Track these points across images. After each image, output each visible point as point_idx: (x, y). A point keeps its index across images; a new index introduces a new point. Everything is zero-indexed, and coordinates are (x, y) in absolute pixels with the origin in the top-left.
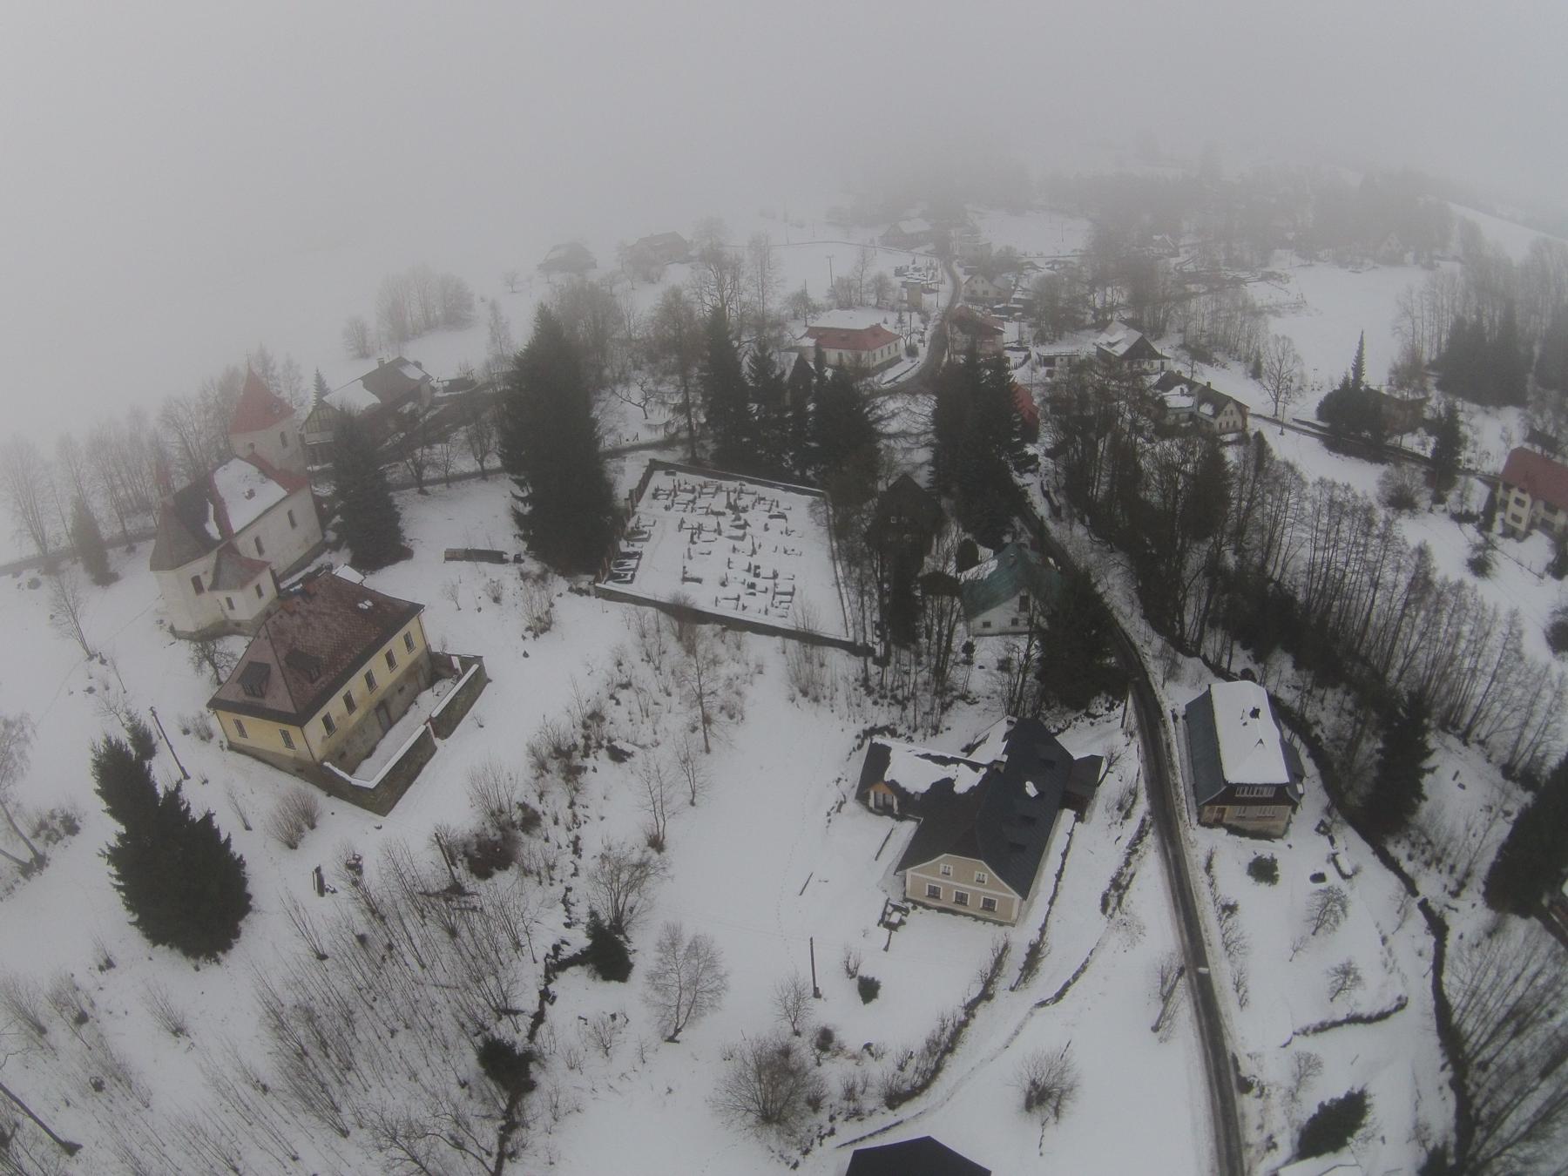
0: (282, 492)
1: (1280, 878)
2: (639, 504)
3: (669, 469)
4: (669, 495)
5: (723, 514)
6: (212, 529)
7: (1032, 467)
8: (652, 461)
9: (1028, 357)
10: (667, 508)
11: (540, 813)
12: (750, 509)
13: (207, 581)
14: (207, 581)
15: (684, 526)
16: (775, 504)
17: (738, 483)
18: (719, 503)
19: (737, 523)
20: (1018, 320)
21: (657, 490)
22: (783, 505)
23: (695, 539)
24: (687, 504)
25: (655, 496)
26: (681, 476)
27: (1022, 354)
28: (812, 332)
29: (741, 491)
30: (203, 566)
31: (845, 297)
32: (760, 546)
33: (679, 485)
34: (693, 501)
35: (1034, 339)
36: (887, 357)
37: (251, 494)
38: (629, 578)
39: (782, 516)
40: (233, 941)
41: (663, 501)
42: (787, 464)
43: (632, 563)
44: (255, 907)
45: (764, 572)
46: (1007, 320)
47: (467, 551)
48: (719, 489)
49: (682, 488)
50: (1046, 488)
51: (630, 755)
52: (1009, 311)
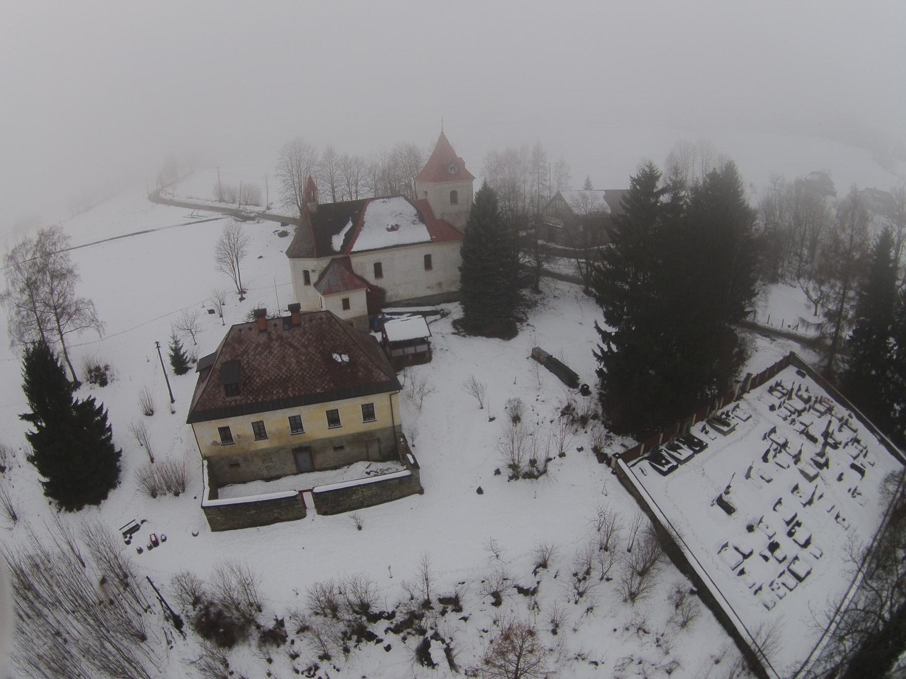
0: (427, 237)
1: (778, 542)
2: (752, 391)
3: (803, 369)
4: (784, 395)
5: (813, 440)
6: (338, 242)
8: (792, 354)
10: (772, 408)
11: (289, 640)
12: (841, 447)
13: (314, 278)
14: (314, 278)
15: (773, 436)
16: (864, 451)
17: (849, 412)
18: (817, 428)
19: (819, 459)
21: (778, 384)
22: (871, 457)
23: (770, 456)
24: (792, 413)
25: (771, 390)
26: (808, 382)
29: (846, 423)
30: (315, 265)
32: (821, 496)
33: (799, 389)
34: (800, 413)
37: (394, 228)
38: (665, 469)
39: (862, 472)
40: (75, 510)
41: (775, 399)
42: (895, 414)
43: (685, 452)
44: (101, 506)
45: (801, 535)
47: (550, 357)
48: (830, 410)
49: (799, 393)
51: (431, 664)
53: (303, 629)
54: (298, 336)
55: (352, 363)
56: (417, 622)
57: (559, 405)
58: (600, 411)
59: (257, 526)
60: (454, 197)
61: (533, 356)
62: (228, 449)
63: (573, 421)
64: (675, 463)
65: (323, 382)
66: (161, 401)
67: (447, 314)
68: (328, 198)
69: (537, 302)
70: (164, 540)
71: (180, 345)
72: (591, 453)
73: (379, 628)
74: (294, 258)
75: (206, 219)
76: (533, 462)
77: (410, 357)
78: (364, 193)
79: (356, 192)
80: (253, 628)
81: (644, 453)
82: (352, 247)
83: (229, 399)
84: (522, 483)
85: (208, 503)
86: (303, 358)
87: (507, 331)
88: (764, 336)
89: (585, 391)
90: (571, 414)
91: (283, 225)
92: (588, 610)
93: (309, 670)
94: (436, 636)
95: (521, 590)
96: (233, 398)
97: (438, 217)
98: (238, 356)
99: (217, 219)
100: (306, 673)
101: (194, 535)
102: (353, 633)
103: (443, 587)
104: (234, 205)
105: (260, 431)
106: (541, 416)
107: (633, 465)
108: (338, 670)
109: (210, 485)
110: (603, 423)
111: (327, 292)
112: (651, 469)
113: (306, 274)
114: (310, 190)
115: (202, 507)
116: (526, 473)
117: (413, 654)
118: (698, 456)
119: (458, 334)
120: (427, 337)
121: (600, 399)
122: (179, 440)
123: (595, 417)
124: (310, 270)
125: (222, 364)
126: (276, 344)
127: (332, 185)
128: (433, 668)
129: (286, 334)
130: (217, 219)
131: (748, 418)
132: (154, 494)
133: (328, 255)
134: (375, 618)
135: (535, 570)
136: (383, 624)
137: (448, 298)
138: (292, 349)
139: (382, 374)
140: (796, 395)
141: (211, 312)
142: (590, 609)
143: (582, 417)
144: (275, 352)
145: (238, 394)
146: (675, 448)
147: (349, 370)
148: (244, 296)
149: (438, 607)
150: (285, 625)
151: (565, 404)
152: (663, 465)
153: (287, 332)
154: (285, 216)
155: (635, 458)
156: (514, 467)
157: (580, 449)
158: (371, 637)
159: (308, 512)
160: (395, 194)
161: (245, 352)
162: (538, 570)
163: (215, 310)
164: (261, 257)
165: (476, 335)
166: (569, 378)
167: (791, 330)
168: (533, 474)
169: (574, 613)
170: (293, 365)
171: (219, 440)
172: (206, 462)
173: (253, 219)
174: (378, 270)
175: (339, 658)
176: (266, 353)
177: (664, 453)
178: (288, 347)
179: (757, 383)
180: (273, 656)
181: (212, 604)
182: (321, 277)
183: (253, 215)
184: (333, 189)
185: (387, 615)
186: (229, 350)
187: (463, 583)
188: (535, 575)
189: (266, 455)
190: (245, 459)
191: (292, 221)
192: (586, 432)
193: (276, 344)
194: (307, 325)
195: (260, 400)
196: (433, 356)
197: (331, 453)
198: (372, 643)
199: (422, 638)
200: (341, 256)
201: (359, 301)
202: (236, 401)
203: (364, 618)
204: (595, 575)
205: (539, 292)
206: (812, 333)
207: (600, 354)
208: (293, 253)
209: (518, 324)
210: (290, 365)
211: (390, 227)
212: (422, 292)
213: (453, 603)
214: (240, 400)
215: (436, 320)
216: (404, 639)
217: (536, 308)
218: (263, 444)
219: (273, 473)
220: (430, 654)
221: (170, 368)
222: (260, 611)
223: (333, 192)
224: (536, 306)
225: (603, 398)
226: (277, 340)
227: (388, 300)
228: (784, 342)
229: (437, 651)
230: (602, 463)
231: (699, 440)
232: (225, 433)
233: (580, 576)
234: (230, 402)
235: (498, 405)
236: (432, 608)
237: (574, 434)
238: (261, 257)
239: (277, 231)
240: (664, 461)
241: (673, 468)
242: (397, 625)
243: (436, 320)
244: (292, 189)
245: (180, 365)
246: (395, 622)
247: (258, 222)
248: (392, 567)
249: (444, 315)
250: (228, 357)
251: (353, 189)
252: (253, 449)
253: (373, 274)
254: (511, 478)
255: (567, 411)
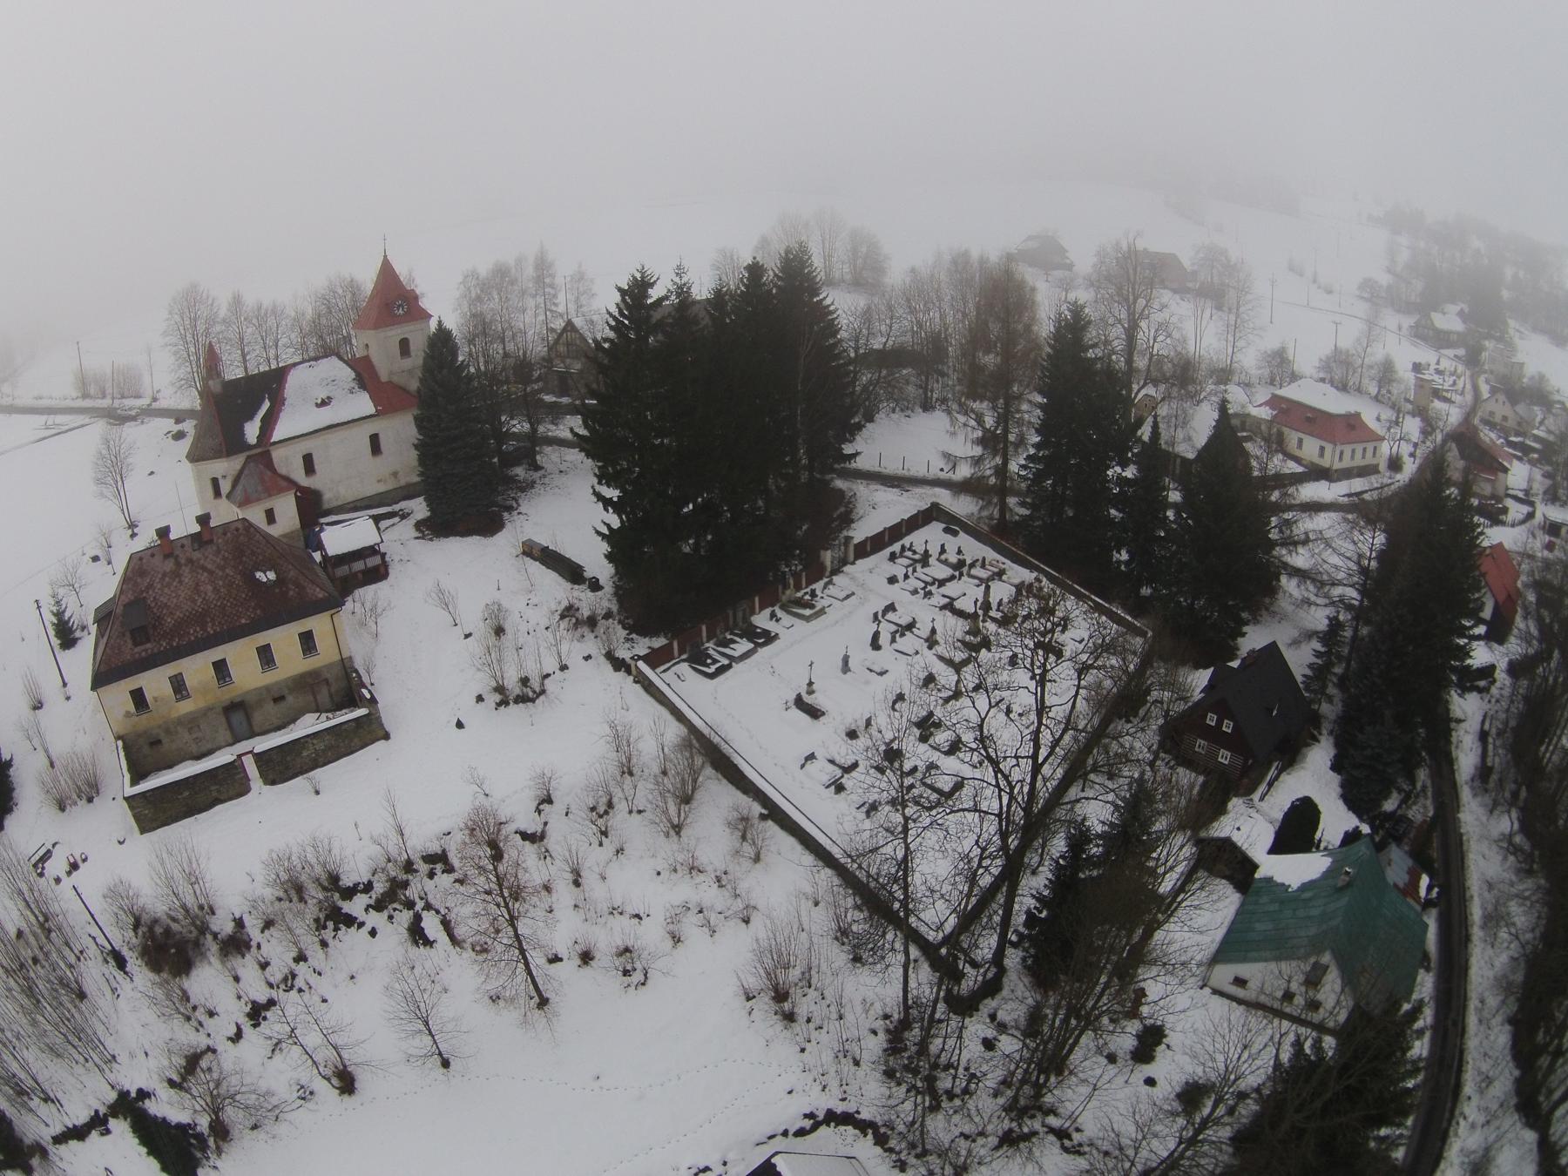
2: (858, 562)
3: (953, 524)
6: (252, 431)
7: (1482, 683)
9: (1531, 516)
10: (892, 580)
11: (254, 943)
13: (225, 487)
14: (225, 487)
17: (1035, 574)
20: (1532, 463)
26: (964, 540)
27: (1525, 509)
28: (1274, 402)
30: (226, 468)
31: (1340, 371)
35: (1545, 493)
36: (1358, 461)
37: (324, 403)
38: (712, 669)
43: (743, 646)
46: (1519, 459)
47: (545, 550)
50: (1487, 727)
51: (429, 943)
52: (1526, 450)
53: (268, 924)
54: (211, 556)
55: (280, 581)
56: (400, 892)
57: (554, 607)
58: (615, 608)
59: (193, 815)
60: (404, 346)
61: (524, 553)
62: (144, 721)
63: (578, 624)
64: (726, 662)
65: (248, 610)
66: (50, 687)
67: (409, 514)
68: (237, 371)
69: (535, 482)
70: (84, 860)
71: (64, 607)
72: (603, 659)
73: (356, 906)
74: (197, 461)
75: (67, 428)
76: (525, 681)
77: (360, 576)
78: (287, 357)
79: (277, 357)
80: (209, 937)
81: (680, 655)
82: (271, 436)
83: (137, 650)
84: (514, 710)
85: (131, 791)
86: (221, 583)
87: (487, 523)
88: (889, 487)
89: (595, 586)
90: (573, 616)
91: (178, 421)
92: (618, 852)
93: (285, 979)
94: (428, 907)
95: (525, 836)
96: (142, 647)
97: (384, 378)
98: (142, 592)
99: (82, 426)
100: (283, 986)
101: (121, 843)
102: (327, 918)
103: (421, 840)
104: (104, 401)
105: (178, 685)
106: (532, 622)
107: (664, 671)
108: (320, 974)
109: (129, 770)
110: (620, 622)
111: (245, 502)
112: (693, 672)
113: (215, 482)
114: (212, 362)
115: (125, 799)
116: (518, 696)
117: (405, 934)
118: (764, 652)
119: (423, 538)
120: (378, 544)
121: (616, 594)
122: (82, 731)
123: (608, 615)
124: (219, 477)
125: (125, 606)
126: (186, 570)
127: (243, 350)
128: (431, 947)
129: (196, 555)
130: (82, 426)
131: (848, 597)
132: (62, 808)
133: (241, 452)
134: (349, 893)
135: (537, 808)
136: (360, 902)
137: (408, 493)
138: (206, 574)
139: (318, 589)
140: (938, 560)
141: (95, 559)
142: (620, 851)
143: (588, 618)
144: (187, 580)
145: (148, 640)
146: (726, 643)
147: (277, 590)
148: (136, 530)
149: (423, 868)
150: (246, 924)
151: (565, 603)
152: (708, 666)
153: (196, 552)
154: (179, 407)
155: (669, 661)
156: (500, 689)
157: (588, 658)
158: (350, 921)
159: (252, 784)
160: (327, 352)
161: (150, 586)
162: (541, 807)
163: (100, 555)
164: (152, 473)
165: (447, 536)
166: (572, 572)
167: (943, 475)
168: (528, 697)
169: (594, 858)
170: (209, 594)
171: (132, 708)
172: (120, 743)
173: (134, 418)
174: (309, 464)
175: (316, 955)
176: (175, 584)
177: (711, 652)
178: (201, 571)
179: (869, 549)
180: (241, 972)
181: (156, 921)
182: (234, 485)
183: (133, 413)
184: (244, 355)
185: (362, 886)
186: (130, 586)
187: (449, 833)
188: (539, 814)
189: (191, 722)
190: (168, 731)
191: (190, 414)
192: (596, 637)
193: (186, 570)
194: (220, 541)
195: (175, 644)
196: (390, 571)
197: (270, 707)
198: (353, 929)
199: (411, 912)
200: (259, 450)
201: (287, 511)
202: (146, 650)
203: (337, 895)
204: (621, 807)
205: (538, 468)
206: (964, 472)
207: (606, 531)
208: (195, 457)
209: (505, 514)
210: (206, 594)
211: (319, 401)
212: (372, 488)
213: (438, 860)
214: (152, 649)
215: (393, 525)
216: (391, 917)
217: (533, 491)
218: (186, 707)
219: (204, 749)
220: (423, 929)
221: (56, 642)
222: (213, 913)
223: (245, 361)
224: (533, 487)
225: (621, 592)
226: (186, 565)
227: (326, 506)
228: (923, 491)
229: (431, 925)
230: (620, 670)
231: (764, 630)
232: (138, 697)
233: (601, 809)
234: (140, 654)
235: (473, 616)
236: (416, 871)
237: (578, 641)
238: (152, 473)
239: (169, 432)
240: (709, 661)
241: (722, 670)
242: (378, 901)
243: (393, 525)
244: (188, 364)
245: (66, 636)
246: (374, 897)
247: (142, 422)
248: (359, 823)
249: (404, 516)
250: (130, 596)
251: (272, 353)
252: (174, 715)
253: (303, 471)
254: (499, 705)
255: (569, 612)
